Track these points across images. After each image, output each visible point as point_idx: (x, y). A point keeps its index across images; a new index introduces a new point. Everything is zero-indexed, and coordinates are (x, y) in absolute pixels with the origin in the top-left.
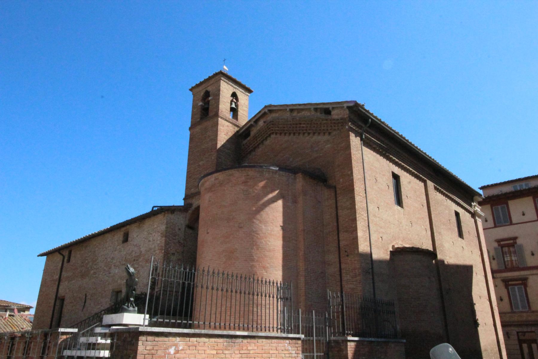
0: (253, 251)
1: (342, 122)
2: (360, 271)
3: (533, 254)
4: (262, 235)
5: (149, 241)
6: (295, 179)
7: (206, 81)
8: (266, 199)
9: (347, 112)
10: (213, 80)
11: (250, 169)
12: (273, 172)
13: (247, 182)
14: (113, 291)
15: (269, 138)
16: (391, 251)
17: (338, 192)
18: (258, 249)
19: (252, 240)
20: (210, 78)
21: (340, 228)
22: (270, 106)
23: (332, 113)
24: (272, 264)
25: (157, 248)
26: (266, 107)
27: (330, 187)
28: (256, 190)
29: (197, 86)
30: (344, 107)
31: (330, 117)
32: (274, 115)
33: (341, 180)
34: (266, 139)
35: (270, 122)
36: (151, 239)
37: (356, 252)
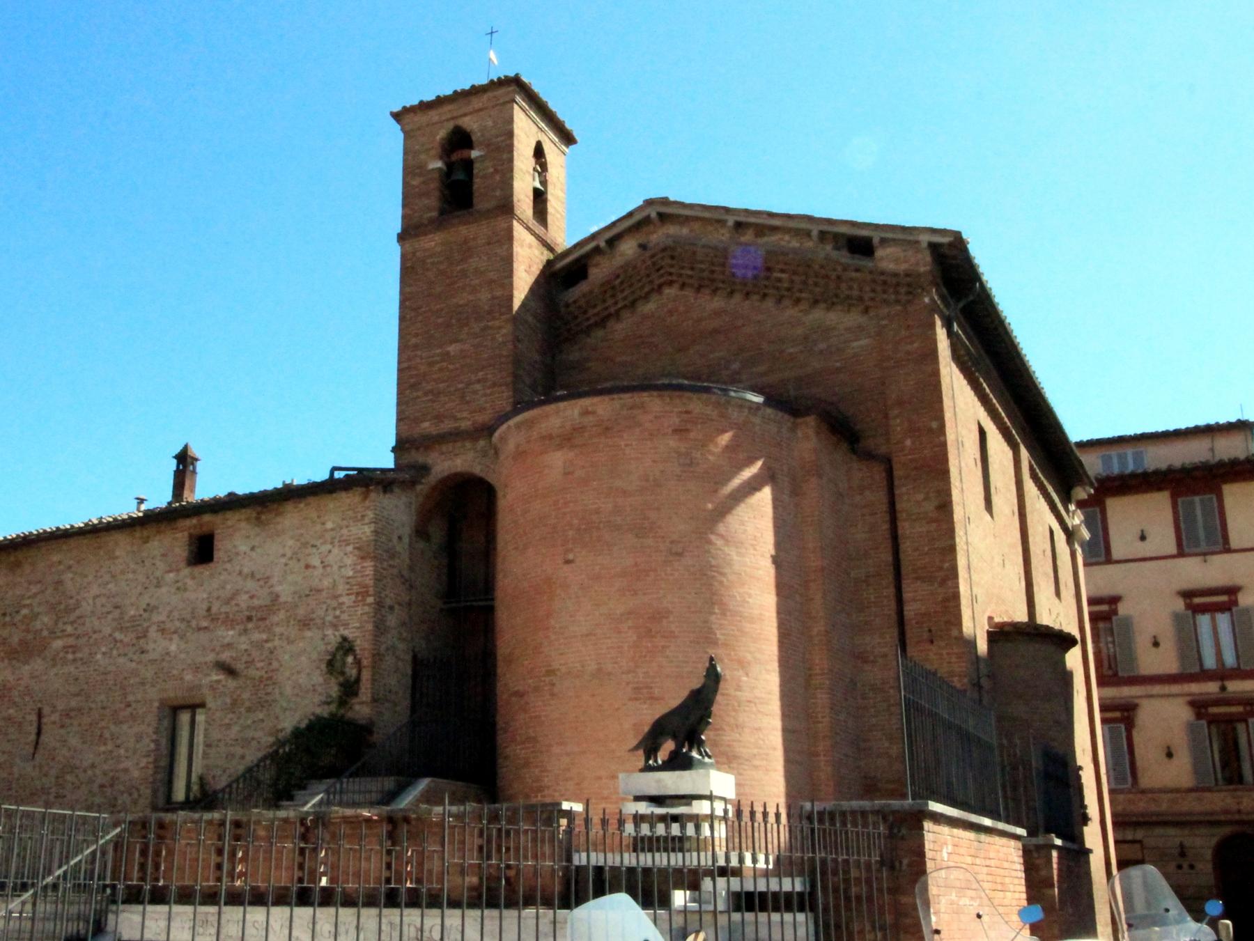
0: (713, 618)
1: (906, 285)
2: (966, 680)
3: (1156, 644)
4: (732, 577)
5: (307, 567)
6: (793, 429)
7: (458, 96)
8: (736, 482)
9: (927, 257)
10: (485, 97)
11: (695, 396)
12: (750, 408)
13: (687, 430)
14: (163, 703)
15: (654, 297)
16: (988, 632)
17: (898, 472)
18: (725, 615)
19: (708, 587)
20: (475, 91)
21: (905, 570)
22: (665, 201)
23: (880, 253)
24: (758, 656)
25: (342, 588)
26: (649, 203)
27: (868, 456)
28: (713, 454)
29: (424, 106)
30: (917, 242)
31: (866, 263)
32: (672, 229)
33: (908, 442)
34: (646, 297)
35: (664, 250)
36: (315, 561)
37: (955, 633)
